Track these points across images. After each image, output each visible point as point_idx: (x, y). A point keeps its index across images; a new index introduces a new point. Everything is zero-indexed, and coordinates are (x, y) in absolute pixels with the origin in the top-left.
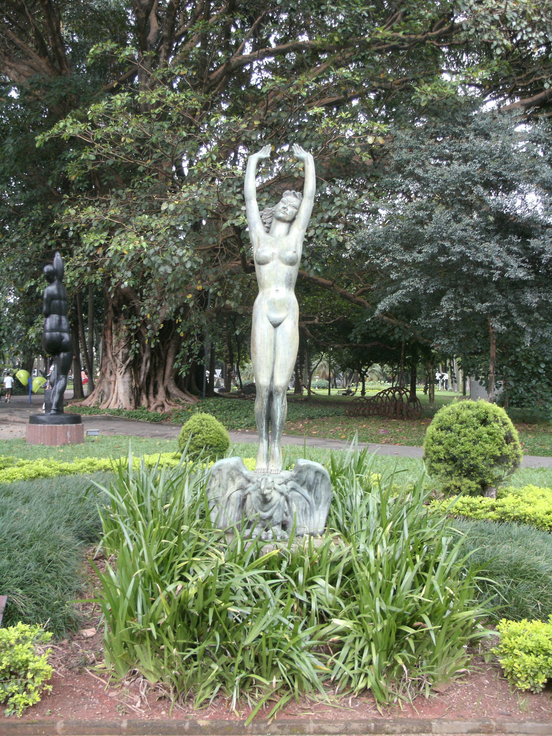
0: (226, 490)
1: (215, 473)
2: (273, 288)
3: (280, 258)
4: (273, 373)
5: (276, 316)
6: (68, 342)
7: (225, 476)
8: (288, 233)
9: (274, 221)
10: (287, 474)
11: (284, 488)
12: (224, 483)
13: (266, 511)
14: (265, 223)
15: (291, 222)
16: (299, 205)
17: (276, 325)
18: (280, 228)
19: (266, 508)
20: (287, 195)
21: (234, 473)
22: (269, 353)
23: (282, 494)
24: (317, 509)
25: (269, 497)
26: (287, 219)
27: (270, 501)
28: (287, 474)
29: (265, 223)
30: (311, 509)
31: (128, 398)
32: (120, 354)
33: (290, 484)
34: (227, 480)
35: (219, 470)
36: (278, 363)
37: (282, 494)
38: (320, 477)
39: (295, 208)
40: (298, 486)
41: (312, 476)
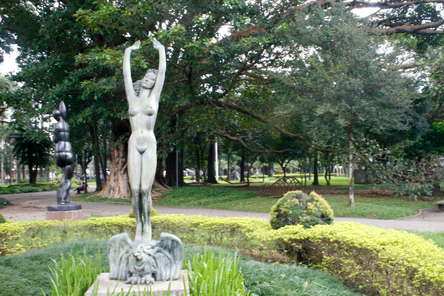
0: (119, 253)
1: (112, 244)
2: (140, 130)
3: (143, 112)
4: (141, 182)
5: (142, 148)
6: (72, 159)
7: (117, 245)
8: (149, 96)
9: (141, 88)
10: (154, 243)
11: (151, 252)
12: (117, 249)
13: (140, 266)
14: (136, 90)
15: (152, 88)
16: (157, 77)
17: (142, 153)
18: (145, 93)
19: (139, 264)
20: (150, 72)
21: (123, 243)
22: (138, 169)
23: (150, 255)
24: (175, 263)
25: (140, 258)
26: (149, 87)
27: (141, 260)
28: (154, 243)
29: (136, 90)
30: (171, 263)
31: (126, 190)
32: (120, 162)
33: (157, 248)
34: (119, 248)
35: (114, 241)
36: (143, 176)
37: (150, 255)
38: (175, 244)
39: (154, 80)
40: (162, 249)
41: (170, 243)
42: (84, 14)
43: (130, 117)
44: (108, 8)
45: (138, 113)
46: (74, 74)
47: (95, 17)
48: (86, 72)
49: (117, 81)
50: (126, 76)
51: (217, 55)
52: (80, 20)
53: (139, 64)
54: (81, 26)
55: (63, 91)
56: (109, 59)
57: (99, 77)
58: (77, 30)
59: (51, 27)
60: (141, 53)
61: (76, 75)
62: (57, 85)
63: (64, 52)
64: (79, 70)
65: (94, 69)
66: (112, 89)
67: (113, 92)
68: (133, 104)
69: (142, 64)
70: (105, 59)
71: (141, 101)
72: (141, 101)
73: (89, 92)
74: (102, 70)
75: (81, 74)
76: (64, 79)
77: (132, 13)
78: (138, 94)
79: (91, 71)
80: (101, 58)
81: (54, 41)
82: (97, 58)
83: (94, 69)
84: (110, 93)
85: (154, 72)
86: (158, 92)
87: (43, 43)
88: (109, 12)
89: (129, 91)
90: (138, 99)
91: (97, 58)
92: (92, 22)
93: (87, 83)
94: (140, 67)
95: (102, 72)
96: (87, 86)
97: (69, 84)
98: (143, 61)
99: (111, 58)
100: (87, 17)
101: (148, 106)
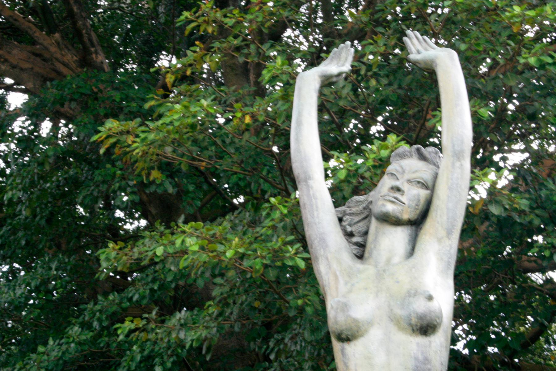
3: (396, 321)
8: (412, 252)
9: (374, 223)
15: (417, 223)
26: (406, 216)
29: (349, 235)
39: (424, 186)
42: (121, 133)
43: (336, 345)
44: (186, 107)
45: (370, 323)
46: (98, 307)
47: (151, 136)
48: (130, 300)
49: (220, 314)
50: (308, 178)
51: (509, 217)
52: (109, 152)
53: (282, 259)
54: (114, 176)
55: (67, 357)
56: (196, 248)
57: (167, 310)
58: (103, 188)
59: (33, 184)
60: (284, 228)
61: (101, 311)
62: (51, 342)
63: (69, 253)
64: (111, 297)
65: (152, 290)
66: (206, 339)
67: (208, 349)
68: (343, 288)
69: (291, 258)
70: (184, 252)
71: (380, 276)
72: (380, 276)
73: (138, 358)
74: (172, 293)
75: (114, 308)
76: (69, 323)
77: (253, 116)
78: (361, 252)
79: (143, 297)
80: (170, 250)
81: (43, 222)
82: (160, 251)
83: (152, 290)
84: (200, 348)
85: (422, 157)
86: (449, 233)
87: (14, 231)
88: (190, 121)
89: (323, 240)
90: (366, 270)
91: (160, 251)
92: (145, 153)
93: (133, 326)
94: (284, 266)
95: (174, 298)
96: (134, 336)
97: (83, 337)
98: (292, 250)
99: (202, 248)
100: (130, 139)
101: (413, 294)
